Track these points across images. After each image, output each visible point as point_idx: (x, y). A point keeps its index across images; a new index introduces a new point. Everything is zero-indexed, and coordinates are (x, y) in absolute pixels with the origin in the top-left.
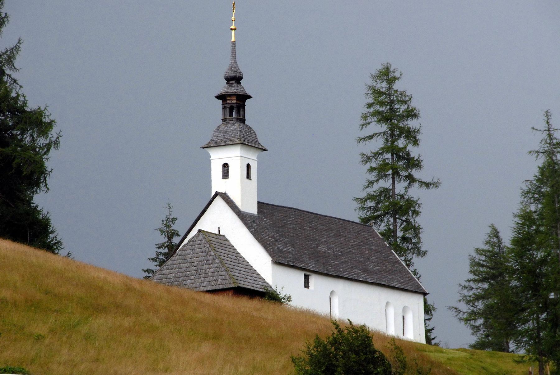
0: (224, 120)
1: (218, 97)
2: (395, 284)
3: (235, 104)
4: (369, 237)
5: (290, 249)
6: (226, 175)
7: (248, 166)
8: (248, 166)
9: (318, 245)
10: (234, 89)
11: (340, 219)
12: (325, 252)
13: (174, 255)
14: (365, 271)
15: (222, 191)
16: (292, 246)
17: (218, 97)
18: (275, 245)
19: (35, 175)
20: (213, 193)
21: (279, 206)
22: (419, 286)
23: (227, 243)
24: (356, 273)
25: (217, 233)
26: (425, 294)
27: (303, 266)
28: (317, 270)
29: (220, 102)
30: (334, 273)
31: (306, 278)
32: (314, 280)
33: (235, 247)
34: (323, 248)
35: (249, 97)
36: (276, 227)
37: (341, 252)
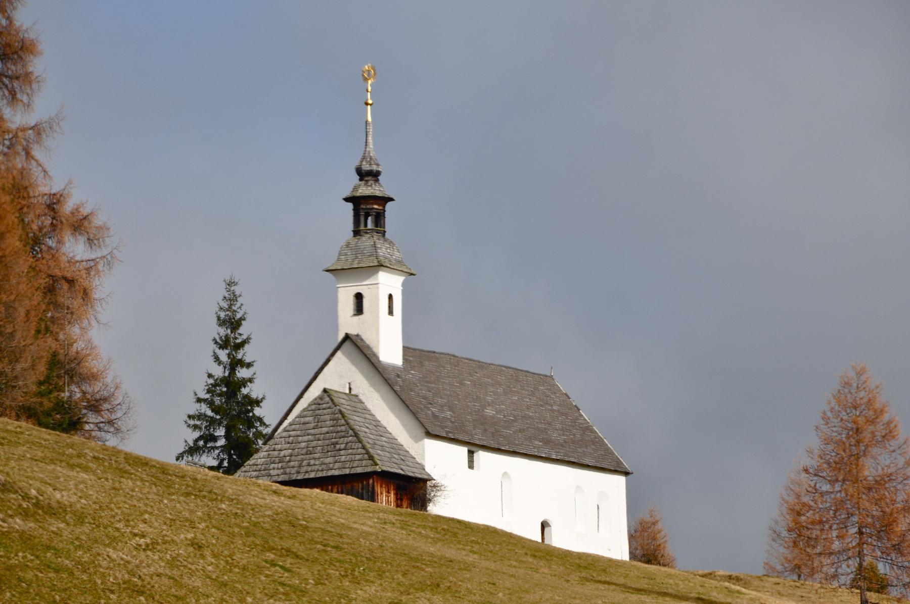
0: (357, 233)
1: (347, 200)
2: (587, 461)
3: (368, 211)
4: (548, 393)
5: (449, 413)
6: (359, 309)
7: (390, 297)
8: (390, 297)
9: (484, 407)
10: (365, 190)
11: (510, 368)
12: (493, 417)
13: (378, 469)
14: (547, 442)
15: (353, 332)
16: (451, 409)
17: (347, 200)
18: (428, 409)
19: (63, 292)
20: (341, 336)
21: (429, 352)
22: (619, 463)
23: (359, 405)
24: (536, 446)
25: (347, 392)
26: (626, 474)
27: (466, 439)
28: (485, 443)
29: (350, 206)
30: (507, 448)
31: (471, 453)
32: (482, 456)
33: (373, 412)
34: (489, 412)
35: (391, 200)
36: (427, 382)
37: (514, 417)
